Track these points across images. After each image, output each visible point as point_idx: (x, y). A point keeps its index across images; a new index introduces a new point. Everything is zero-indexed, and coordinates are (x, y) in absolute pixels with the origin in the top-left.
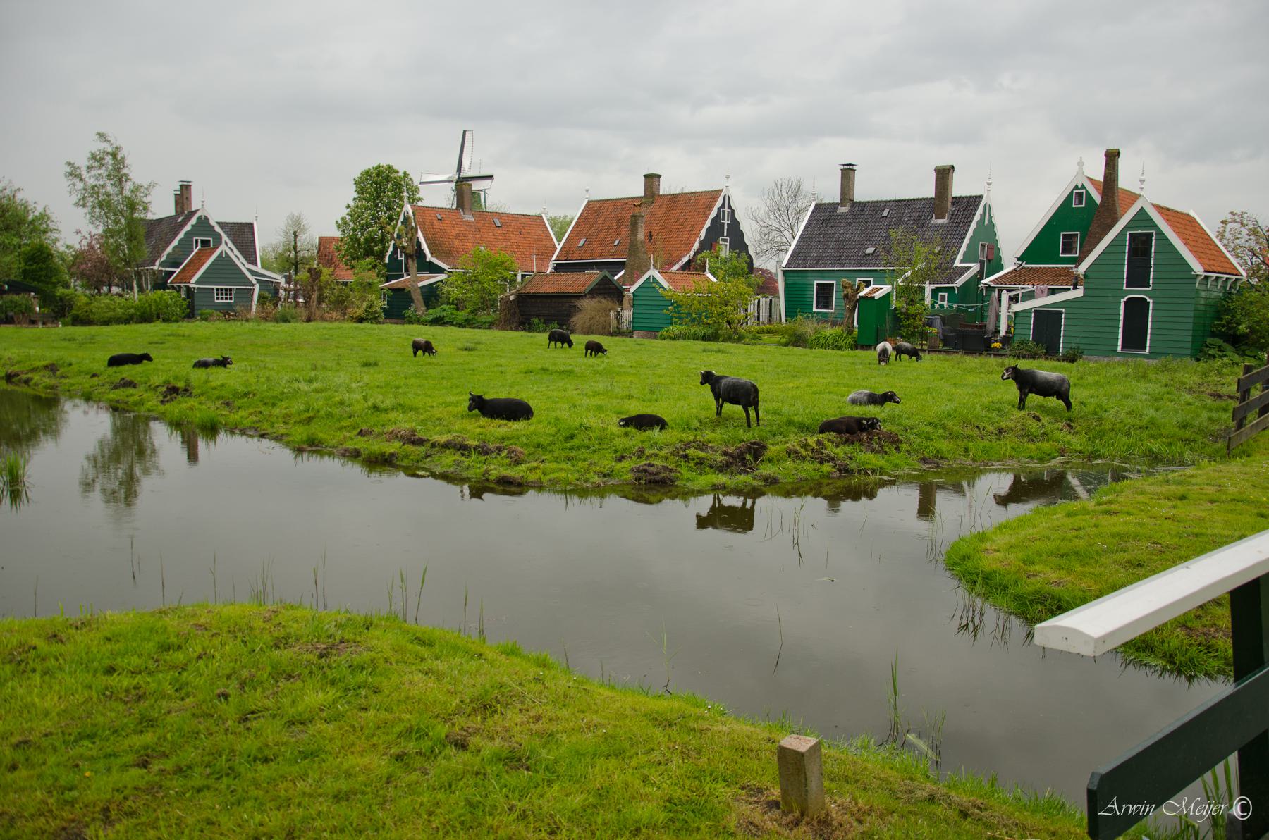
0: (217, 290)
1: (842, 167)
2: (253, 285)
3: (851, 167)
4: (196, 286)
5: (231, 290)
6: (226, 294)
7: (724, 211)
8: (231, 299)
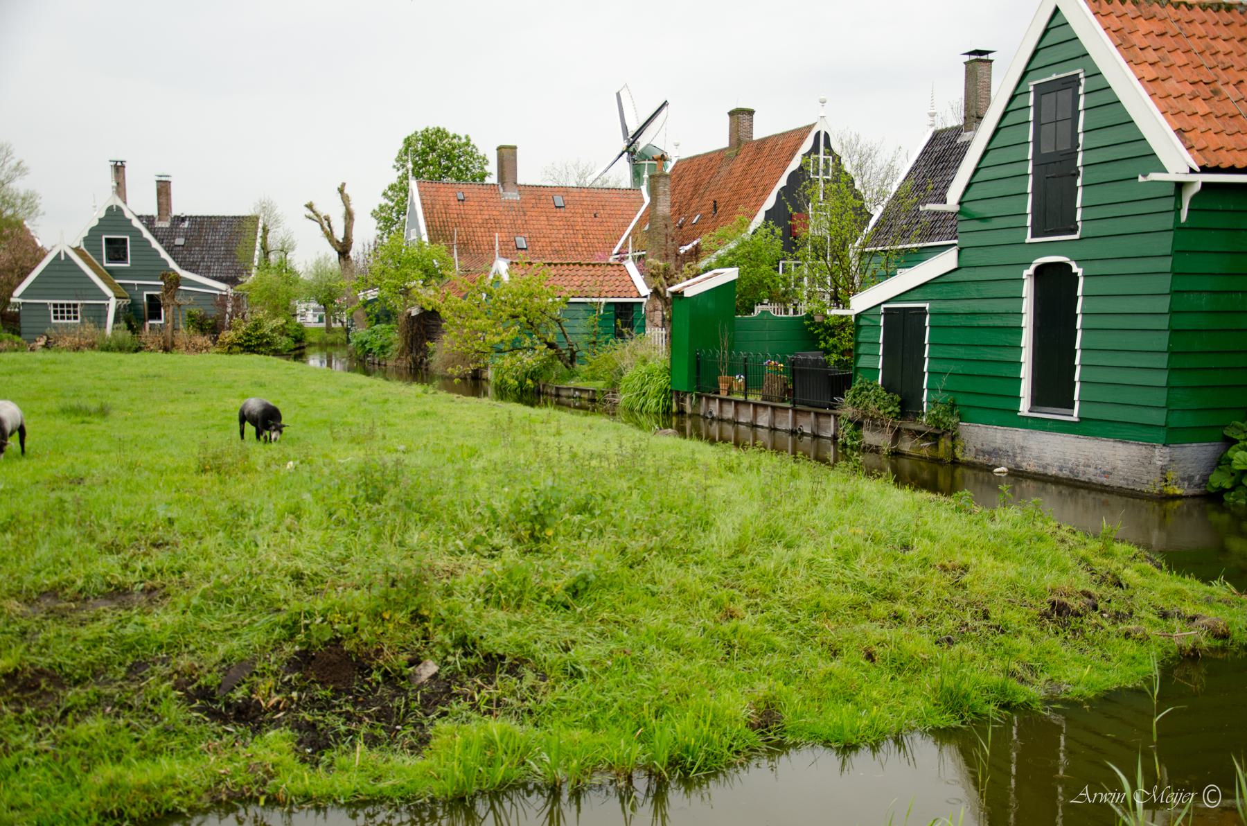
0: (55, 305)
1: (967, 58)
2: (108, 299)
3: (984, 57)
4: (21, 301)
5: (75, 306)
6: (69, 312)
7: (817, 161)
8: (76, 318)
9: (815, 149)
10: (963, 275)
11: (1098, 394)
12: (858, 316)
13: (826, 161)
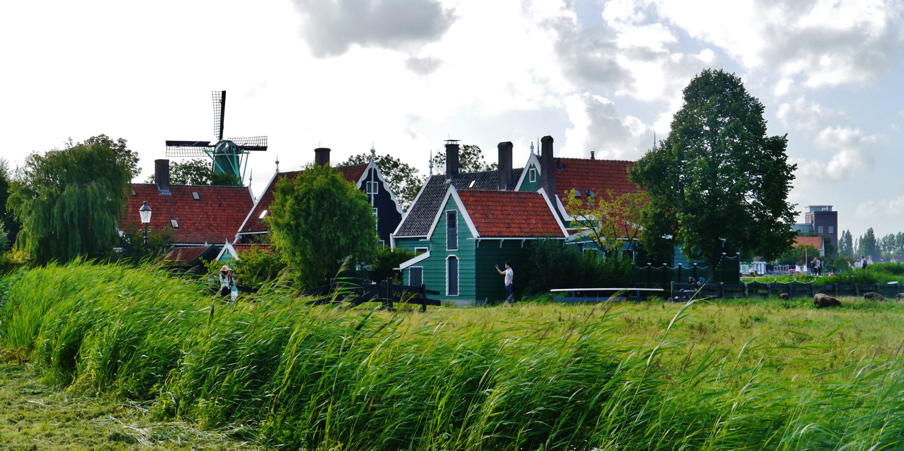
1: (446, 143)
7: (370, 184)
9: (369, 178)
10: (432, 259)
11: (463, 289)
12: (402, 270)
13: (375, 185)
